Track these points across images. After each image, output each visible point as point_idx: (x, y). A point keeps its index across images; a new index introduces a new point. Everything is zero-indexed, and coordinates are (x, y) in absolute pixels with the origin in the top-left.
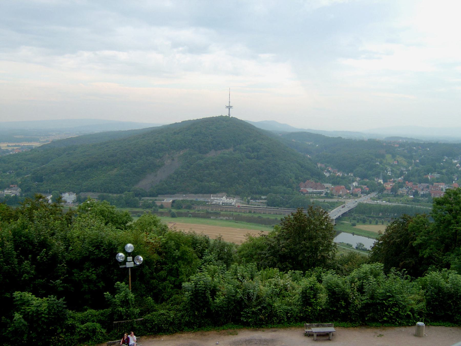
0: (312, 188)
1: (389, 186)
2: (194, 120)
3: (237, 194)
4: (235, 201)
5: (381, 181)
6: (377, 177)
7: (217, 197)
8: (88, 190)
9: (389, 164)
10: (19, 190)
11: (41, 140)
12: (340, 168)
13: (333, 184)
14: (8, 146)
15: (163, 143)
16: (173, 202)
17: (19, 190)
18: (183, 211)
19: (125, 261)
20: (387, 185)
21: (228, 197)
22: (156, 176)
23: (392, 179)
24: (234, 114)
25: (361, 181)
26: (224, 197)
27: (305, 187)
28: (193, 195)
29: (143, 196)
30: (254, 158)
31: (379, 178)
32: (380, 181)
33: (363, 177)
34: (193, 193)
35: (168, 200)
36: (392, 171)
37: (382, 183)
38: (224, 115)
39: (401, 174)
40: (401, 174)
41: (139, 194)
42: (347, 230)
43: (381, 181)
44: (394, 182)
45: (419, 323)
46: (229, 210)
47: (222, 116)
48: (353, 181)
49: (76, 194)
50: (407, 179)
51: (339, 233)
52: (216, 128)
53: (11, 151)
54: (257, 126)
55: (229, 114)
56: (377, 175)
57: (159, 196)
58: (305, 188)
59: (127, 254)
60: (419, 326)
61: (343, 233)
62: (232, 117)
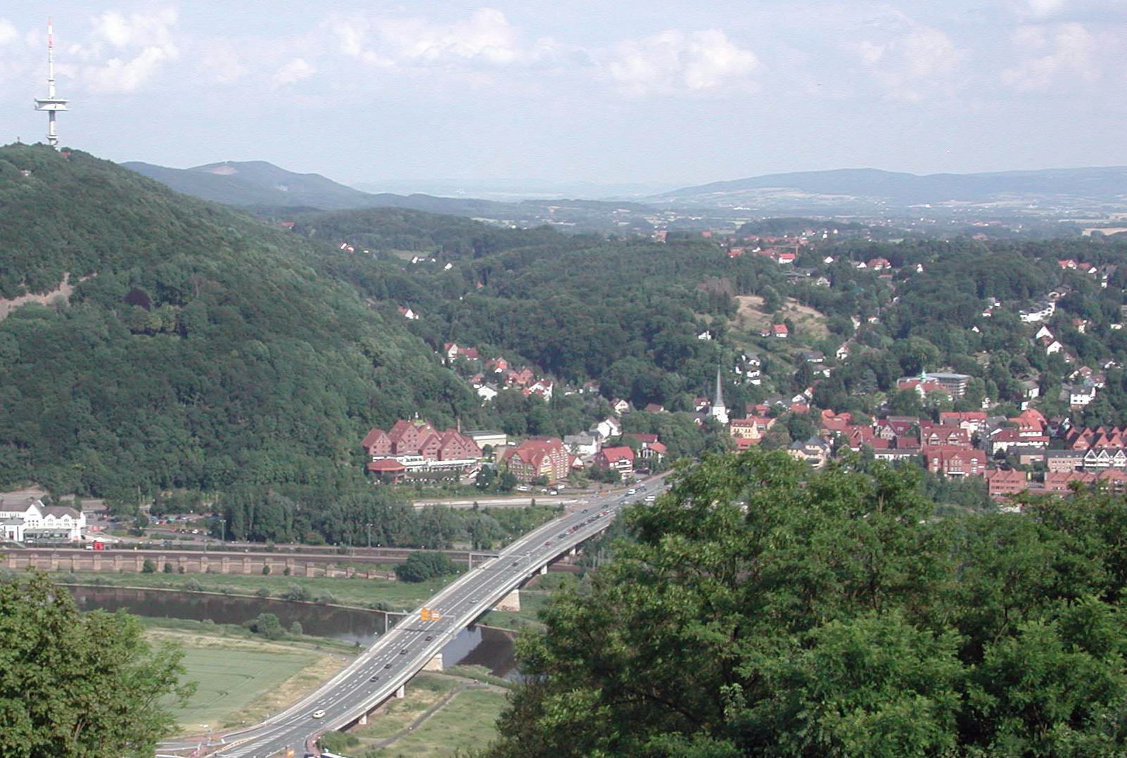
62: (66, 150)
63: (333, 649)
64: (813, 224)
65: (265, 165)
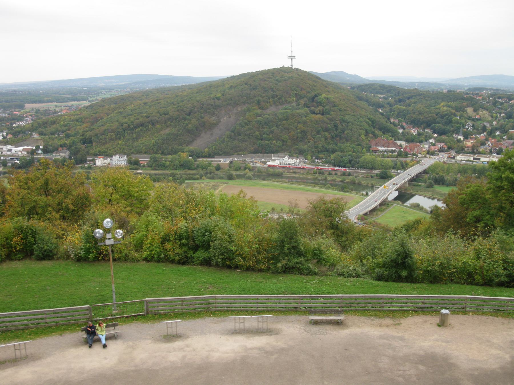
0: (383, 146)
1: (469, 143)
2: (252, 73)
3: (300, 153)
4: (298, 161)
5: (461, 138)
6: (456, 133)
7: (278, 157)
8: (140, 152)
9: (470, 118)
10: (68, 153)
11: (90, 99)
12: (415, 123)
13: (407, 141)
14: (56, 106)
15: (218, 99)
16: (231, 162)
17: (68, 153)
18: (241, 172)
19: (104, 239)
20: (467, 143)
21: (290, 156)
22: (212, 134)
23: (474, 136)
24: (297, 65)
25: (439, 137)
26: (286, 157)
27: (376, 145)
28: (253, 155)
29: (198, 157)
30: (319, 114)
31: (459, 135)
32: (459, 137)
33: (441, 133)
34: (251, 153)
35: (224, 161)
36: (473, 126)
37: (462, 139)
38: (286, 66)
39: (484, 129)
40: (484, 129)
41: (196, 155)
42: (423, 193)
43: (461, 138)
44: (476, 138)
45: (444, 311)
46: (291, 171)
47: (283, 67)
48: (430, 139)
49: (127, 157)
50: (491, 133)
51: (412, 196)
52: (277, 80)
53: (60, 112)
54: (323, 78)
55: (292, 65)
56: (457, 131)
57: (216, 156)
58: (376, 146)
59: (107, 231)
60: (443, 315)
61: (417, 196)
62: (295, 68)
63: (287, 181)
64: (487, 89)
65: (342, 73)
